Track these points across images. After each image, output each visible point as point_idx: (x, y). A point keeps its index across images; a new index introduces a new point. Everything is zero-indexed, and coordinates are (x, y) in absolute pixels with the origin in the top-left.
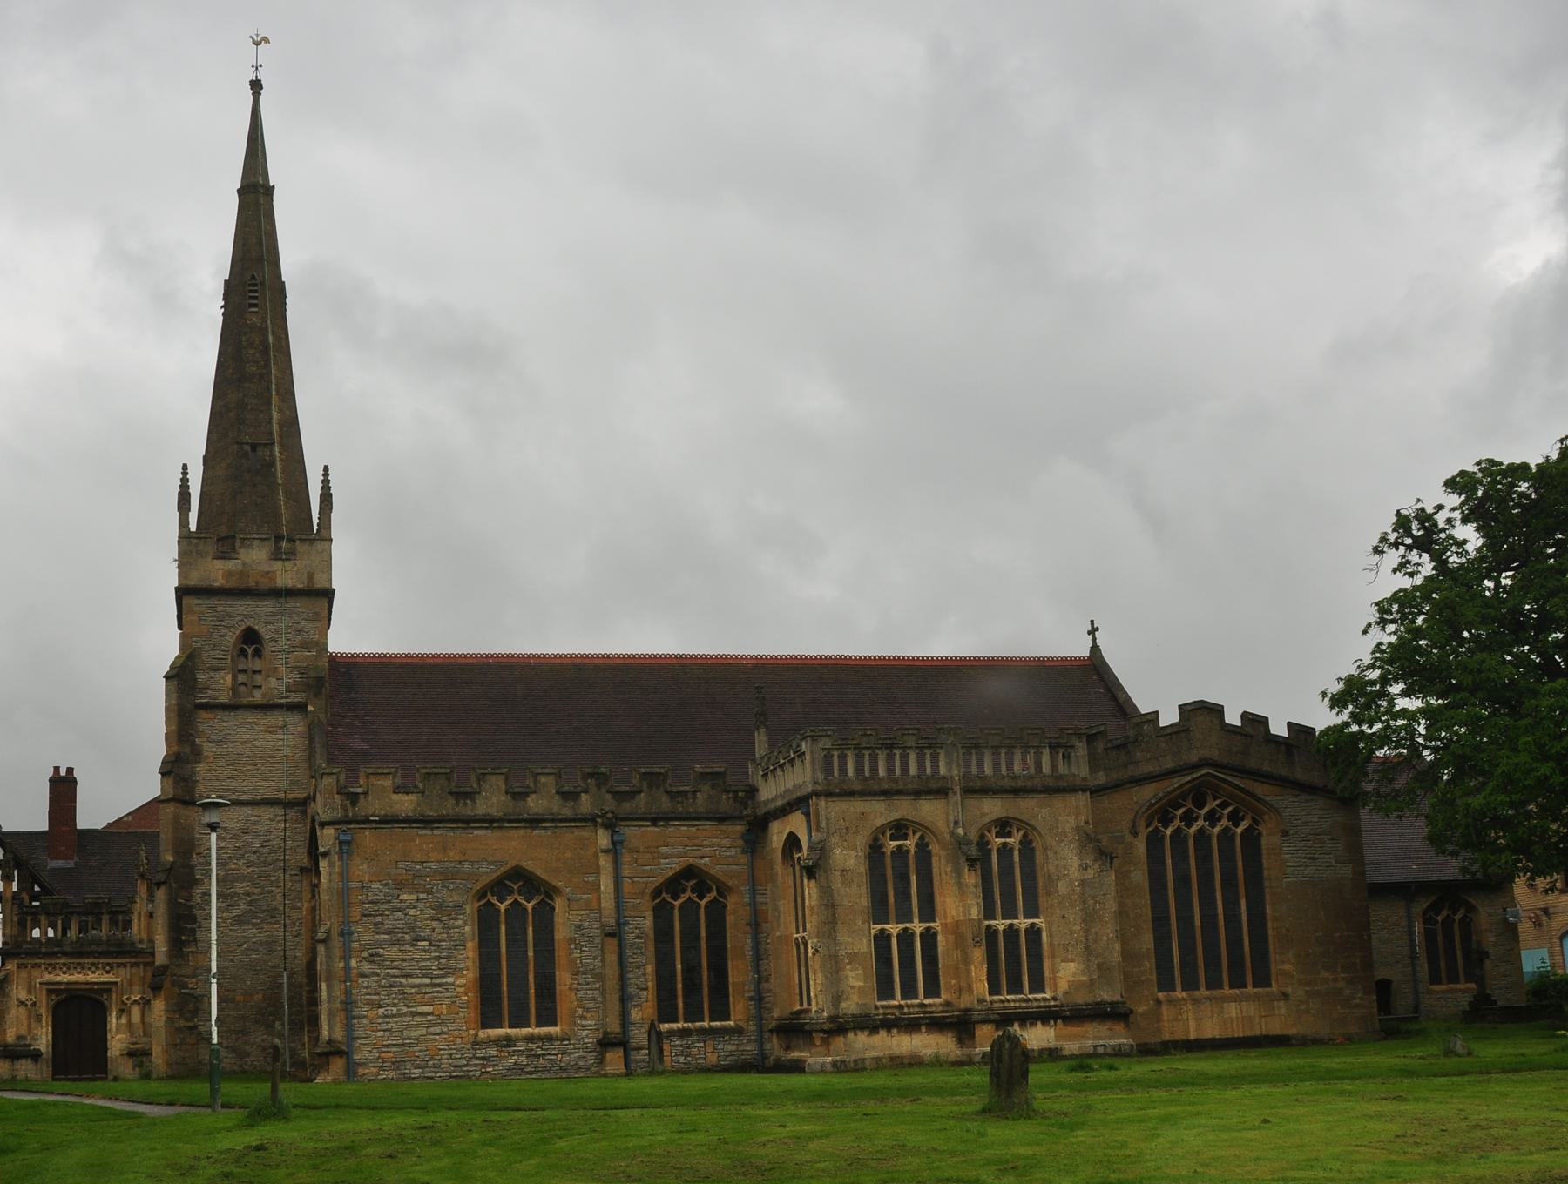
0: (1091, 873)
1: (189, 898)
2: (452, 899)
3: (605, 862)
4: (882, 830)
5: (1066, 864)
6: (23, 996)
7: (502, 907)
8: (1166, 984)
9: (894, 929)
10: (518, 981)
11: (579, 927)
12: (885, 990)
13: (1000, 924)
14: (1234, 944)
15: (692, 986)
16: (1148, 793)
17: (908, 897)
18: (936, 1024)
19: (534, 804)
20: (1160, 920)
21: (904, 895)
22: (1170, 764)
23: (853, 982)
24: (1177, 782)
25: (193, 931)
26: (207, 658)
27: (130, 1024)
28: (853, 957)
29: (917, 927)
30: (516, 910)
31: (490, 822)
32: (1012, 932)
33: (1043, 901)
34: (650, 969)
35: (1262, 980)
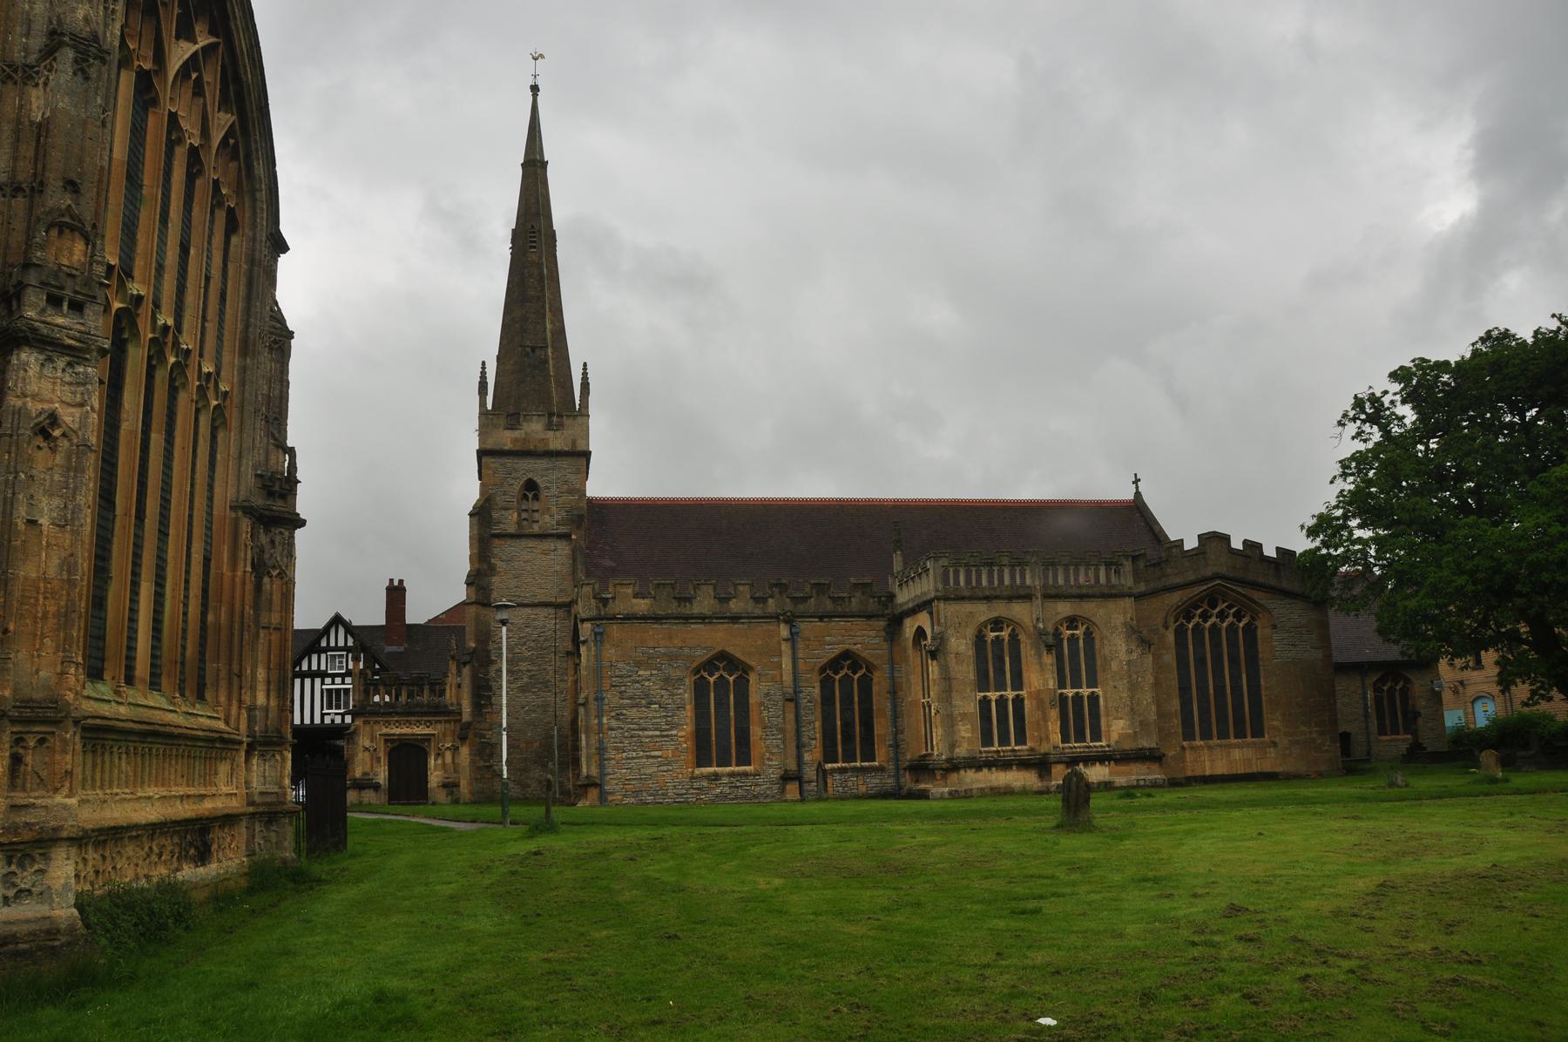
0: (1134, 656)
3: (785, 647)
4: (984, 624)
5: (1117, 649)
7: (712, 680)
8: (1188, 735)
9: (993, 695)
12: (987, 739)
13: (1070, 692)
14: (1238, 706)
16: (1175, 598)
18: (1024, 764)
19: (735, 606)
20: (1184, 690)
21: (1000, 671)
22: (1191, 577)
25: (489, 698)
26: (500, 500)
28: (964, 716)
29: (1010, 694)
31: (703, 619)
33: (1100, 676)
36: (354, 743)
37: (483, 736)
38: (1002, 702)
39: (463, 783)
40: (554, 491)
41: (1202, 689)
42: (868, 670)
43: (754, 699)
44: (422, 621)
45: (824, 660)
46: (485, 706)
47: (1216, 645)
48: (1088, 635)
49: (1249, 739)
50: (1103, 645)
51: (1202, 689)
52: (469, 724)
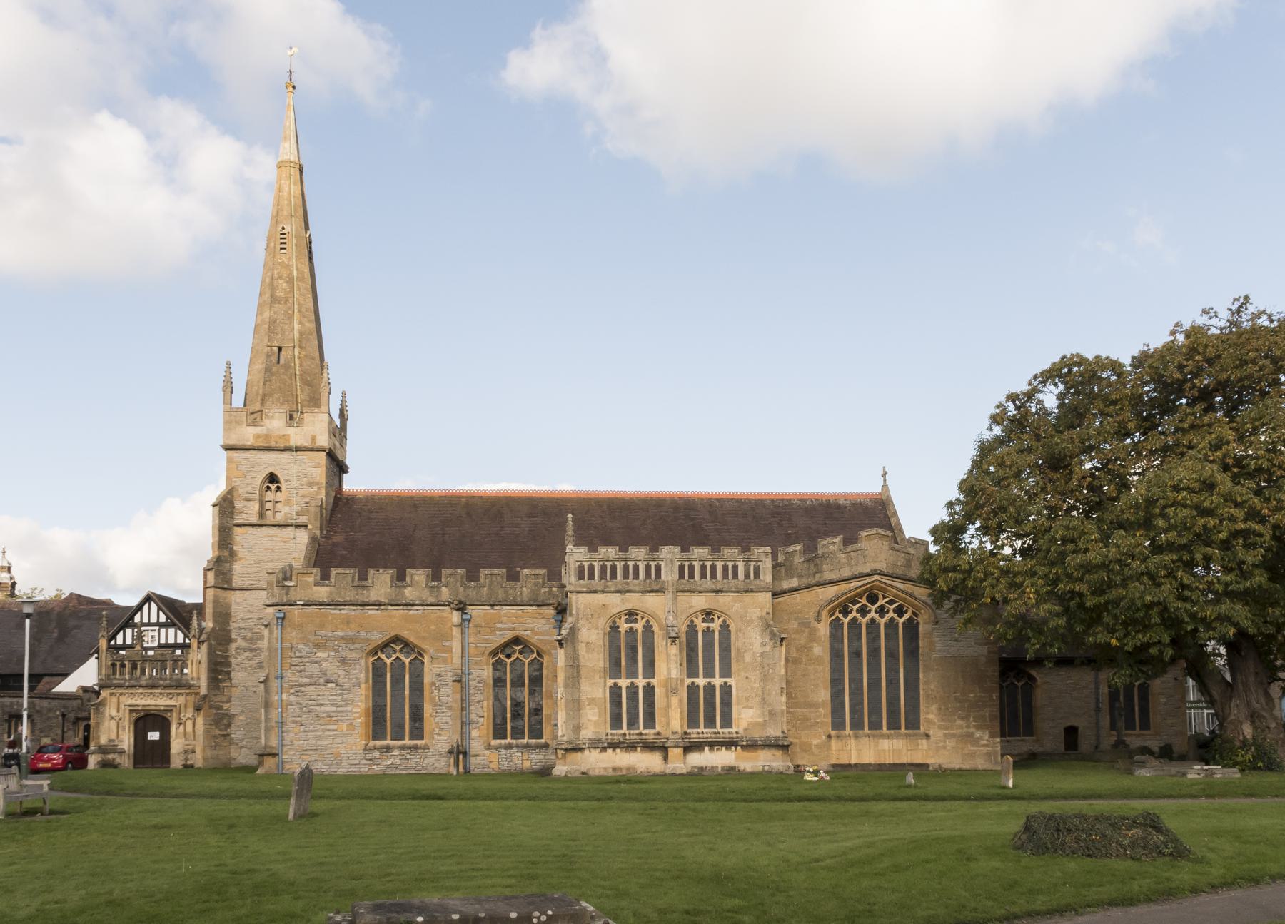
0: (768, 648)
1: (227, 650)
2: (354, 655)
3: (456, 632)
4: (619, 615)
5: (752, 643)
6: (114, 713)
7: (389, 662)
8: (838, 723)
9: (624, 683)
10: (397, 710)
11: (439, 675)
12: (616, 721)
13: (701, 681)
14: (893, 699)
16: (832, 591)
17: (636, 661)
18: (649, 747)
19: (409, 594)
20: (836, 681)
21: (633, 660)
22: (847, 573)
23: (591, 718)
24: (853, 584)
25: (229, 673)
26: (242, 491)
27: (185, 733)
28: (592, 701)
29: (641, 682)
30: (398, 663)
31: (378, 604)
32: (710, 689)
33: (734, 667)
34: (485, 704)
35: (913, 723)
36: (103, 713)
37: (220, 708)
38: (633, 690)
39: (198, 750)
40: (294, 484)
41: (856, 681)
42: (539, 654)
43: (427, 680)
46: (221, 681)
47: (873, 640)
48: (725, 627)
49: (509, 740)
50: (737, 638)
51: (856, 681)
52: (205, 697)
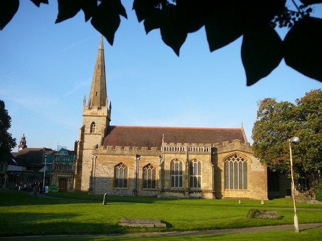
4: (174, 159)
9: (175, 176)
12: (173, 185)
14: (241, 182)
15: (236, 182)
18: (180, 192)
24: (231, 153)
26: (87, 126)
28: (167, 180)
38: (177, 177)
44: (191, 37)
45: (144, 165)
